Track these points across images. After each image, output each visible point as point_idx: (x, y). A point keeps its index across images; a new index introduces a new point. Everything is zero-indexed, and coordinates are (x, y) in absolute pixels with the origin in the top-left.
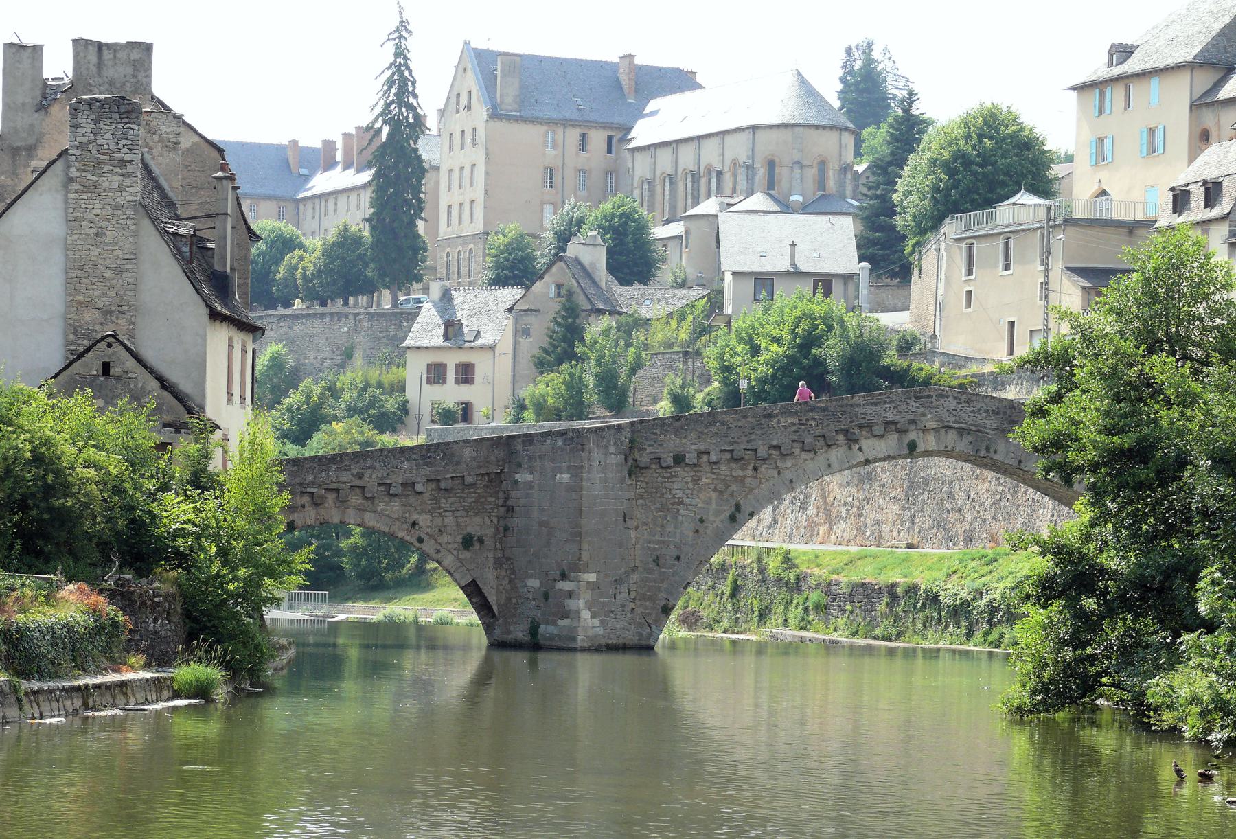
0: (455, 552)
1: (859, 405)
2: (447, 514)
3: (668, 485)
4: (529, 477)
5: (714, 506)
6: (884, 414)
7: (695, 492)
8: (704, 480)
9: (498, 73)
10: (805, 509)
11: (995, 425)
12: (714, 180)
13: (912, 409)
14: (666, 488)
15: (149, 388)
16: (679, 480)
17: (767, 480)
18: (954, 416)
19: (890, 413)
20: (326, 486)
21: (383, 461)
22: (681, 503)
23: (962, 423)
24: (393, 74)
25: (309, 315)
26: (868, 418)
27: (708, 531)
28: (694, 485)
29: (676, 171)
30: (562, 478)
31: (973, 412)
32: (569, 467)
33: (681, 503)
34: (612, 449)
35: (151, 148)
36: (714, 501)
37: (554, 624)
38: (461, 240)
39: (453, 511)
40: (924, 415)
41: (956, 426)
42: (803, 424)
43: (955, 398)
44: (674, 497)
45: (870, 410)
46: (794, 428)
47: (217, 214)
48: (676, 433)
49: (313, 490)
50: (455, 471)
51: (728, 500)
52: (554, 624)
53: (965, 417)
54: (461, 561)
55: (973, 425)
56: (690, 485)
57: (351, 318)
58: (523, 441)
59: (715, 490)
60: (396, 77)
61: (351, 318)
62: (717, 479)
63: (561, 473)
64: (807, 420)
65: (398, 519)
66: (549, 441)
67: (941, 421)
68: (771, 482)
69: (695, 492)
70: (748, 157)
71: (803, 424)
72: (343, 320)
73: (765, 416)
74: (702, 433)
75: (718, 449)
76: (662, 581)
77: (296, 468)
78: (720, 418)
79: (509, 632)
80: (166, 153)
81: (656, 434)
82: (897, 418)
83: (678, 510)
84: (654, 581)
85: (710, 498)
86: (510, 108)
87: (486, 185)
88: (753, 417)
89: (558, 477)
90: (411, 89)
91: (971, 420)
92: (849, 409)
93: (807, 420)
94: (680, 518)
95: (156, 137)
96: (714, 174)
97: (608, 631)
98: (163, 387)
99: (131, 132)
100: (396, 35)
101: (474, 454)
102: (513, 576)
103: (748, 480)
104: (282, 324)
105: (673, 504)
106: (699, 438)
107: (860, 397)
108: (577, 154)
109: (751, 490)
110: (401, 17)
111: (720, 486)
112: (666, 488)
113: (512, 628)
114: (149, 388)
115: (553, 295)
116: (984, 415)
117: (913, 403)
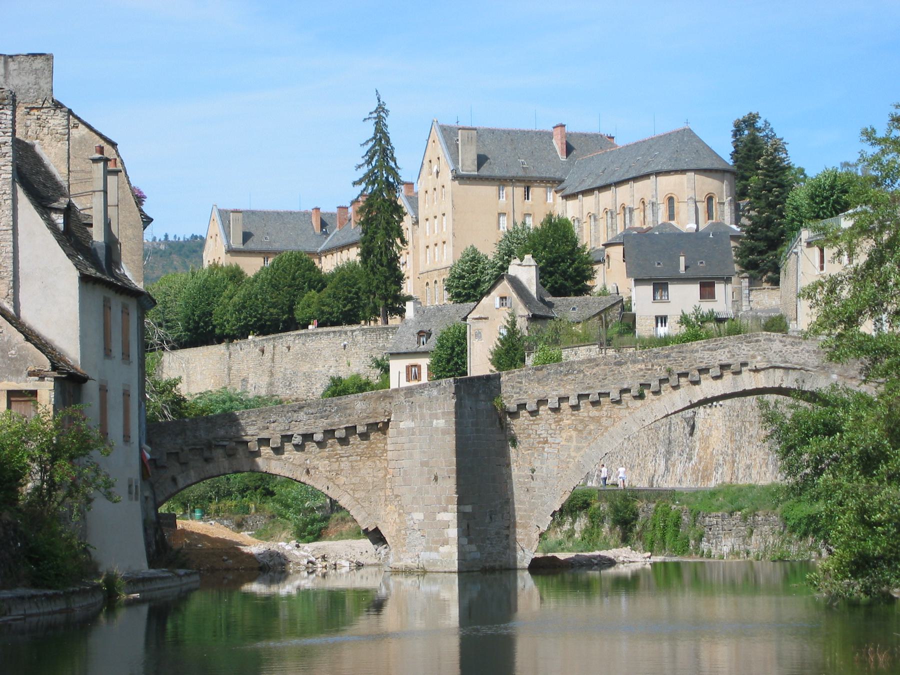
0: (351, 492)
1: (697, 351)
2: (343, 459)
3: (533, 427)
4: (412, 425)
5: (574, 443)
6: (719, 357)
7: (558, 432)
8: (566, 422)
9: (459, 143)
10: (691, 459)
11: (816, 364)
12: (628, 215)
13: (744, 352)
14: (532, 430)
15: (15, 341)
16: (543, 422)
17: (620, 419)
18: (780, 356)
19: (724, 356)
20: (236, 440)
21: (285, 416)
22: (546, 442)
23: (787, 362)
24: (374, 146)
25: (317, 334)
26: (705, 361)
27: (570, 465)
28: (556, 426)
29: (599, 210)
30: (437, 424)
31: (797, 352)
32: (443, 413)
33: (546, 442)
34: (482, 397)
35: (42, 140)
36: (575, 439)
37: (437, 550)
38: (436, 272)
39: (347, 457)
40: (754, 357)
41: (783, 365)
42: (649, 370)
43: (781, 341)
44: (540, 437)
45: (706, 354)
46: (642, 373)
47: (94, 192)
48: (539, 381)
49: (225, 443)
50: (348, 422)
51: (586, 438)
52: (437, 550)
53: (790, 357)
54: (357, 500)
55: (797, 364)
56: (553, 426)
57: (349, 334)
58: (405, 394)
59: (576, 429)
60: (377, 148)
61: (349, 334)
62: (576, 420)
63: (437, 419)
64: (653, 366)
65: (300, 465)
66: (426, 392)
67: (769, 361)
68: (624, 421)
69: (558, 432)
70: (653, 197)
71: (649, 370)
72: (343, 336)
73: (615, 364)
74: (561, 380)
75: (576, 394)
76: (532, 511)
77: (210, 425)
78: (576, 367)
79: (400, 560)
80: (54, 144)
81: (521, 383)
82: (730, 361)
83: (544, 448)
84: (525, 511)
85: (571, 437)
86: (470, 169)
87: (453, 229)
88: (605, 365)
89: (435, 422)
90: (390, 155)
91: (795, 360)
92: (688, 355)
93: (653, 366)
94: (546, 454)
95: (46, 130)
96: (627, 211)
97: (485, 555)
98: (27, 339)
99: (4, 116)
100: (375, 115)
101: (364, 407)
102: (401, 511)
103: (603, 420)
104: (297, 342)
105: (539, 443)
106: (559, 385)
107: (697, 344)
108: (523, 202)
109: (606, 428)
110: (379, 101)
111: (580, 427)
112: (532, 430)
113: (402, 556)
114: (15, 341)
115: (498, 306)
116: (807, 354)
117: (744, 347)
